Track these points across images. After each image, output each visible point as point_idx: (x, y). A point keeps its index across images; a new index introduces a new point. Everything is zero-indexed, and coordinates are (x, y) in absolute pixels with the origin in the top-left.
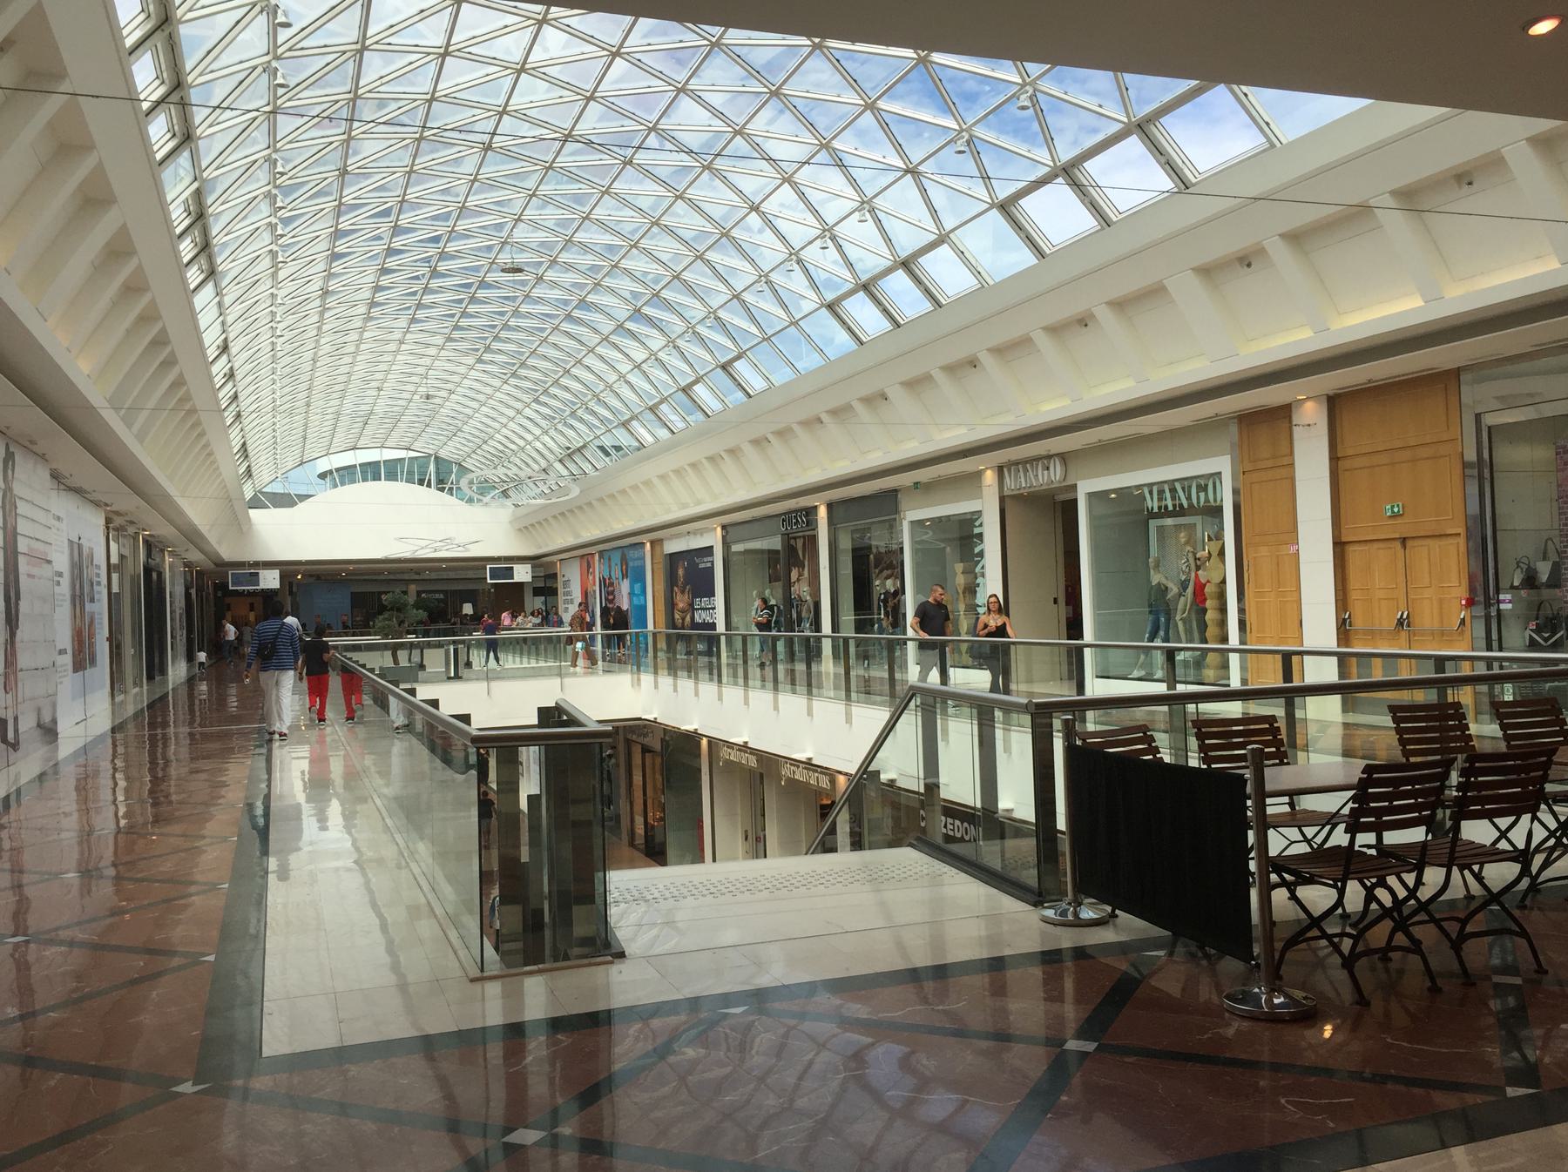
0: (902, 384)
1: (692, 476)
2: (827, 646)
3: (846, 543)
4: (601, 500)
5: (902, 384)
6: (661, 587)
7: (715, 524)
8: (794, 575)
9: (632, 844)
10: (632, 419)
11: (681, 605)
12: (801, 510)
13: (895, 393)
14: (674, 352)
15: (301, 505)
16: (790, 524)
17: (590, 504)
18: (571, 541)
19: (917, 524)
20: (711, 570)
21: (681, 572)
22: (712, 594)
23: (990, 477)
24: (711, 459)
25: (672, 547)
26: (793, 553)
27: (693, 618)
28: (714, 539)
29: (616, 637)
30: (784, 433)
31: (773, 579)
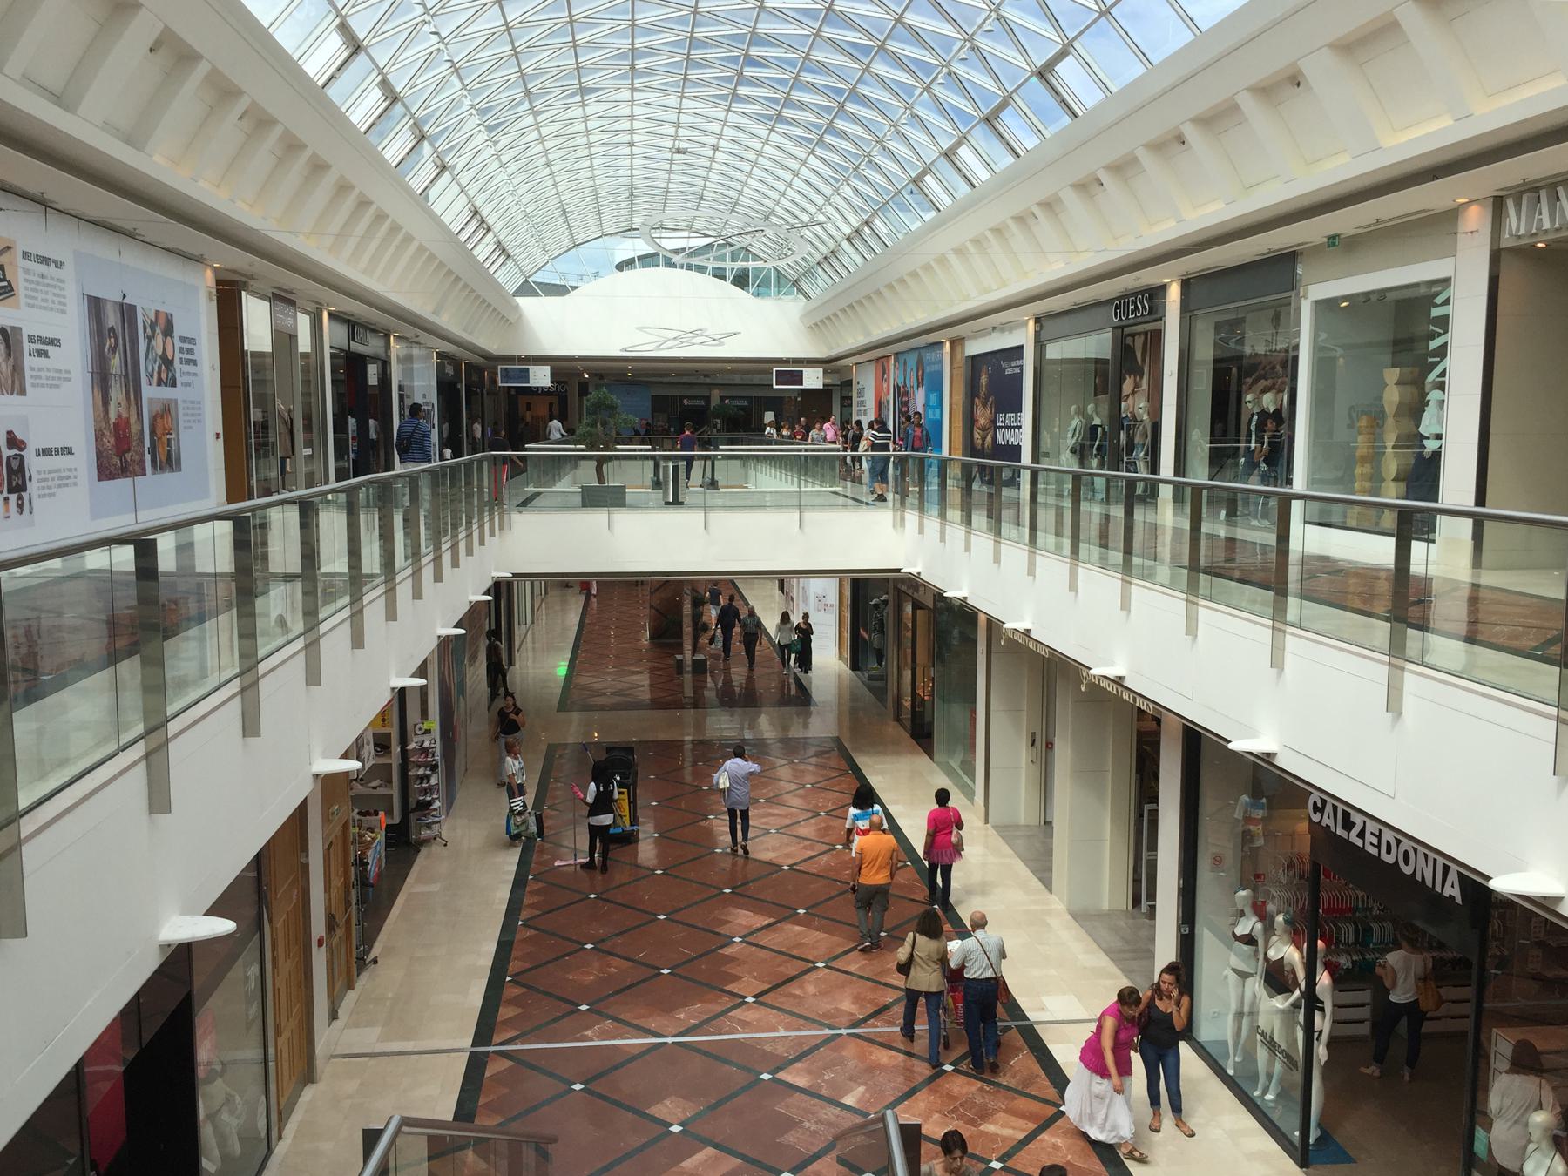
0: (1332, 46)
1: (995, 244)
2: (1166, 492)
3: (1205, 352)
4: (890, 287)
5: (1332, 46)
6: (959, 398)
7: (1027, 314)
8: (1128, 386)
9: (898, 719)
10: (924, 173)
11: (982, 421)
12: (1142, 292)
13: (1320, 69)
14: (973, 57)
15: (573, 293)
16: (1126, 313)
17: (879, 293)
18: (860, 340)
19: (1326, 307)
20: (1018, 378)
21: (984, 380)
22: (1018, 408)
23: (1476, 220)
24: (1020, 219)
25: (975, 348)
26: (1134, 353)
27: (994, 438)
28: (1024, 337)
29: (895, 462)
30: (1123, 168)
31: (1098, 391)
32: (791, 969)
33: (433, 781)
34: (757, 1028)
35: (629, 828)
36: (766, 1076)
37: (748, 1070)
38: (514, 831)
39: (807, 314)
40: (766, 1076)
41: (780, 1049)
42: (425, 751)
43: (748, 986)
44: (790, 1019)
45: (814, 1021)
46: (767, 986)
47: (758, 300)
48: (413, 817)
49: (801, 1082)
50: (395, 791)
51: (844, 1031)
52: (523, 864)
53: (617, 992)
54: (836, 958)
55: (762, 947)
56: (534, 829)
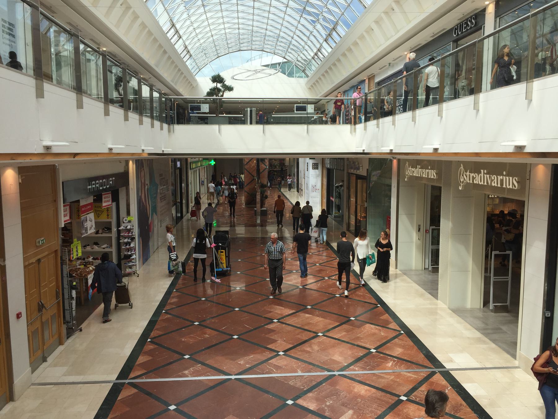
4: (344, 55)
32: (304, 336)
33: (132, 245)
34: (284, 369)
35: (225, 269)
36: (290, 402)
37: (280, 398)
38: (172, 269)
39: (308, 82)
40: (290, 402)
41: (299, 384)
42: (129, 231)
43: (281, 345)
44: (304, 365)
45: (318, 366)
46: (291, 346)
47: (291, 79)
48: (123, 262)
49: (312, 406)
50: (114, 250)
51: (336, 373)
52: (172, 285)
53: (208, 348)
54: (328, 331)
55: (289, 325)
56: (181, 269)
